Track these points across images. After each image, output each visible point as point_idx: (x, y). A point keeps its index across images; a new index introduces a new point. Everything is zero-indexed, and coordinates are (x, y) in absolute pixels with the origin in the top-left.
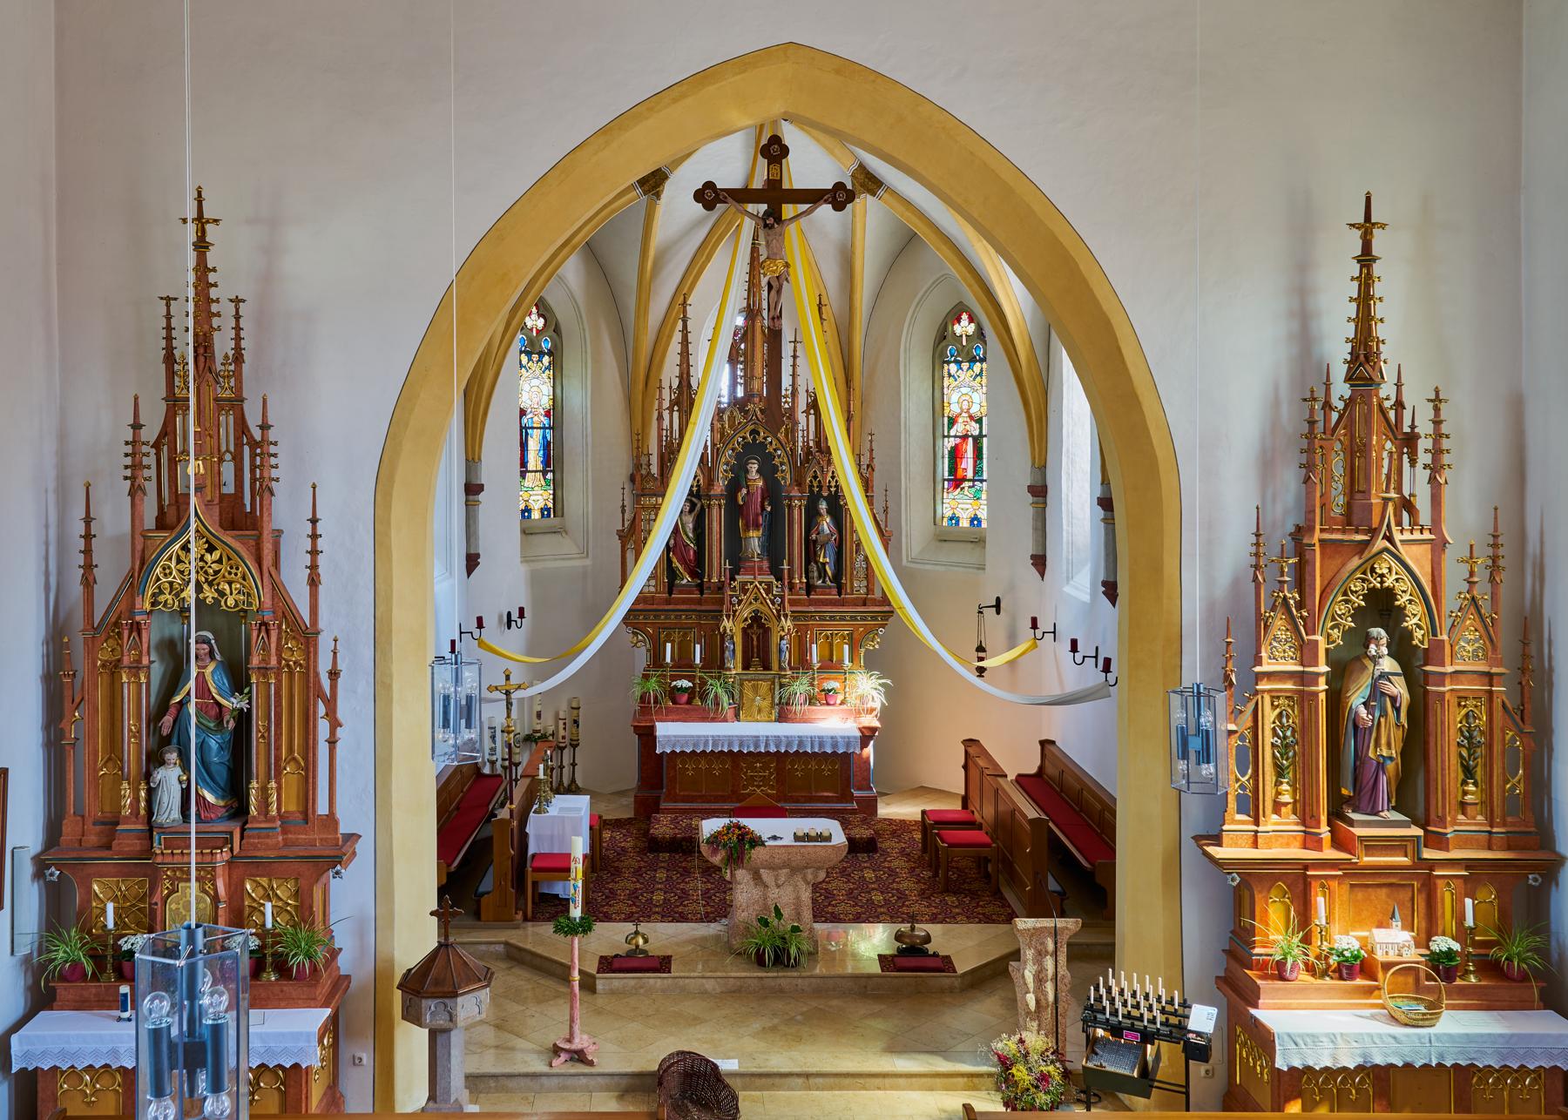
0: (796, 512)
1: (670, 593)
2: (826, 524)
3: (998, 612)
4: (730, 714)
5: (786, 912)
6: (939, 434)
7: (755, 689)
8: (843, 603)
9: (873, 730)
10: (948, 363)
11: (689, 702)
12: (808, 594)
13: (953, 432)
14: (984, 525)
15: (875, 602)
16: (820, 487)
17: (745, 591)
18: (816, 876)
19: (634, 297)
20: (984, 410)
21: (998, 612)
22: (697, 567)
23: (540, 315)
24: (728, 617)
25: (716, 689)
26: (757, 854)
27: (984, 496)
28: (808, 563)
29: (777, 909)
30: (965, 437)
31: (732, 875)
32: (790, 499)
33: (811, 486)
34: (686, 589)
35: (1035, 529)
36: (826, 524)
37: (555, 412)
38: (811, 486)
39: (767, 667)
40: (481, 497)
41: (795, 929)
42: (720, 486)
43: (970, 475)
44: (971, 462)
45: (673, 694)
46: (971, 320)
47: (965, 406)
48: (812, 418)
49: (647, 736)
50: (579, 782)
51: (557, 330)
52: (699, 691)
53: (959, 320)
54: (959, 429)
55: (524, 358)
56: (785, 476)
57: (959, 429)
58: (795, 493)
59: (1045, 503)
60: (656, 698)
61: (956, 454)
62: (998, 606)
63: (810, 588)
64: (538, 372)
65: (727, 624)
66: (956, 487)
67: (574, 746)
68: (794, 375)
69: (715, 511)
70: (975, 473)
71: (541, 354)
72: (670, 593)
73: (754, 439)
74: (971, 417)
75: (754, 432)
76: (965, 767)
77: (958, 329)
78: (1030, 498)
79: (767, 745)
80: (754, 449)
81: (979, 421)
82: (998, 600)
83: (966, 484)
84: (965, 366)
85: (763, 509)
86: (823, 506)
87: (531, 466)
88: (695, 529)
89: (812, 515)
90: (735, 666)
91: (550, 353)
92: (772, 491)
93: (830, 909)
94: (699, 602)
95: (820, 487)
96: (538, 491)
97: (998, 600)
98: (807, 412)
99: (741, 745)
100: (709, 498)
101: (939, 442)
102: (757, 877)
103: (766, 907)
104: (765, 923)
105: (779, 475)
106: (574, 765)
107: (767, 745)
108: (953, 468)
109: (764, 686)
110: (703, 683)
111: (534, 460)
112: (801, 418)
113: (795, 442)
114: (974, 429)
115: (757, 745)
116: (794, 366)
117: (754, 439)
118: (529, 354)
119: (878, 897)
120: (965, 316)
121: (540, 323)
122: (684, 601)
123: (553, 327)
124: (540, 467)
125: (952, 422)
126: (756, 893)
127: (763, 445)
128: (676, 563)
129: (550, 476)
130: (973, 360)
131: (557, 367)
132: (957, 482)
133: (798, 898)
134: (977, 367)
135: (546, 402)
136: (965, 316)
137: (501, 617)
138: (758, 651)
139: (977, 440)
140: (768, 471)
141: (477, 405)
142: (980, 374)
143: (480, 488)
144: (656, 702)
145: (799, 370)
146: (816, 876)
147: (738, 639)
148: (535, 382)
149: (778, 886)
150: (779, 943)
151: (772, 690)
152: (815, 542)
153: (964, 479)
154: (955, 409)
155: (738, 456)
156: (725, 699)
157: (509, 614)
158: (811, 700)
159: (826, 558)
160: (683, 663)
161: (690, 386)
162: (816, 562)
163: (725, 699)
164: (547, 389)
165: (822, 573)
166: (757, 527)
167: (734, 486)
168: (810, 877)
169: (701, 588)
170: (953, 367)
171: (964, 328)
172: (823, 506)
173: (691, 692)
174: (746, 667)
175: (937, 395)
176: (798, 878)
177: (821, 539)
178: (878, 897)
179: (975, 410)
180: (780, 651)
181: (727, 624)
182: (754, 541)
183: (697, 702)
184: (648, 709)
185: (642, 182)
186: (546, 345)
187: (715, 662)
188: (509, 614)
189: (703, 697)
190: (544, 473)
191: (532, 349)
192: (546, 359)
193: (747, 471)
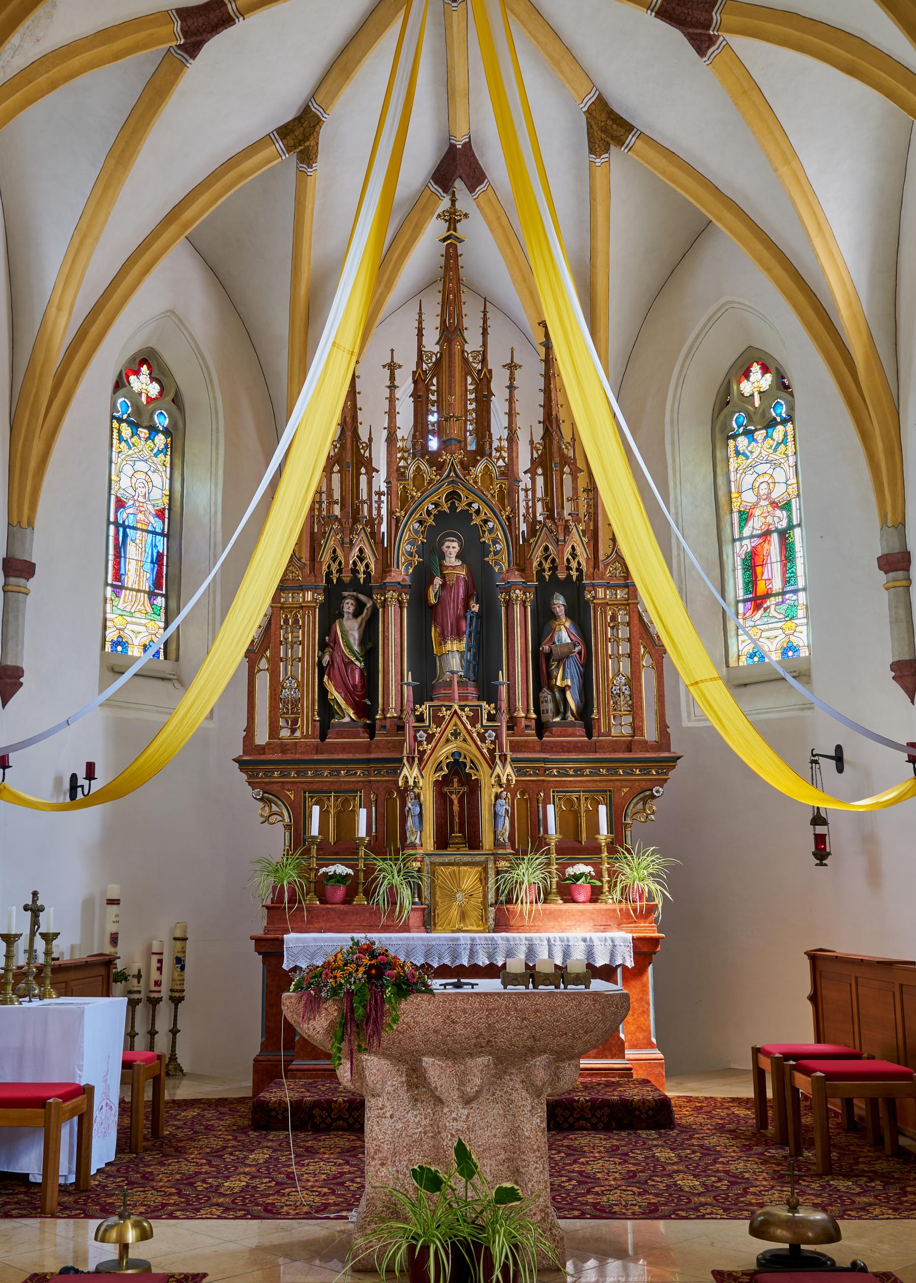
0: (517, 609)
1: (323, 737)
2: (564, 634)
3: (840, 770)
4: (416, 919)
5: (487, 1167)
6: (727, 536)
7: (456, 879)
8: (595, 748)
9: (655, 941)
10: (734, 437)
11: (348, 900)
12: (540, 735)
13: (747, 532)
14: (804, 653)
15: (646, 747)
16: (554, 568)
17: (438, 721)
18: (556, 1077)
19: (285, 352)
20: (793, 490)
21: (840, 770)
22: (366, 697)
23: (152, 379)
24: (411, 760)
25: (390, 875)
26: (413, 1014)
27: (801, 613)
28: (538, 689)
29: (462, 1152)
30: (766, 534)
31: (358, 1072)
32: (508, 590)
33: (541, 570)
34: (347, 730)
35: (894, 621)
36: (564, 634)
37: (172, 515)
38: (541, 570)
39: (474, 843)
40: (32, 584)
41: (506, 1196)
42: (401, 573)
43: (777, 586)
44: (777, 567)
45: (321, 887)
46: (765, 369)
47: (764, 489)
48: (540, 480)
49: (270, 949)
50: (184, 1060)
51: (177, 400)
52: (361, 885)
53: (747, 374)
54: (756, 525)
55: (126, 430)
56: (501, 561)
57: (756, 525)
58: (516, 578)
59: (909, 579)
60: (293, 893)
61: (752, 563)
62: (838, 758)
63: (541, 728)
64: (146, 452)
65: (410, 773)
66: (757, 607)
67: (176, 1000)
68: (511, 414)
69: (392, 610)
70: (786, 581)
71: (153, 430)
72: (323, 737)
73: (453, 507)
74: (774, 505)
75: (453, 496)
76: (814, 998)
77: (746, 387)
78: (882, 577)
79: (472, 954)
80: (451, 520)
81: (787, 506)
82: (839, 748)
83: (772, 601)
84: (760, 435)
85: (467, 607)
86: (559, 603)
87: (130, 580)
88: (362, 642)
89: (543, 621)
90: (424, 837)
91: (167, 432)
92: (481, 584)
93: (590, 1198)
94: (367, 748)
95: (554, 568)
96: (140, 619)
97: (839, 748)
98: (532, 471)
99: (427, 954)
100: (383, 588)
101: (727, 549)
102: (416, 1080)
103: (438, 1155)
104: (433, 1183)
105: (490, 559)
106: (174, 1032)
107: (472, 954)
108: (752, 582)
109: (470, 878)
110: (370, 870)
111: (137, 570)
112: (525, 480)
113: (515, 510)
114: (780, 520)
115: (455, 955)
116: (511, 401)
117: (453, 507)
118: (134, 426)
119: (687, 1182)
120: (756, 368)
121: (154, 389)
122: (344, 748)
123: (173, 398)
124: (146, 585)
125: (745, 516)
126: (415, 1120)
127: (466, 515)
128: (335, 694)
129: (160, 601)
130: (771, 424)
131: (175, 437)
132: (758, 601)
133: (514, 1132)
134: (778, 432)
135: (159, 498)
136: (756, 368)
137: (58, 780)
138: (458, 827)
139: (784, 535)
140: (476, 552)
141: (28, 442)
142: (784, 441)
143: (26, 570)
144: (292, 901)
145: (518, 407)
146: (556, 1077)
147: (428, 797)
148: (141, 466)
149: (467, 1101)
150: (465, 1231)
151: (484, 880)
152: (549, 655)
153: (768, 595)
154: (749, 497)
155: (431, 533)
156: (406, 894)
157: (74, 777)
158: (546, 896)
159: (565, 678)
160: (344, 847)
161: (356, 436)
162: (551, 688)
163: (406, 894)
164: (160, 480)
165: (561, 707)
166: (458, 635)
167: (422, 578)
168: (541, 1075)
169: (371, 730)
170: (742, 442)
171: (757, 382)
172: (559, 603)
173: (351, 886)
174: (442, 842)
175: (721, 480)
176: (514, 1082)
177: (557, 651)
178: (687, 1182)
179: (778, 493)
180: (496, 815)
181: (410, 773)
182: (454, 656)
183: (360, 900)
184: (282, 911)
185: (284, 131)
186: (162, 421)
187: (389, 839)
188: (74, 777)
189: (369, 893)
190: (152, 595)
191: (140, 419)
192: (160, 440)
193: (442, 556)
